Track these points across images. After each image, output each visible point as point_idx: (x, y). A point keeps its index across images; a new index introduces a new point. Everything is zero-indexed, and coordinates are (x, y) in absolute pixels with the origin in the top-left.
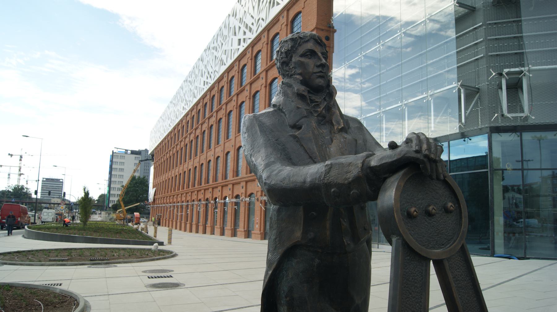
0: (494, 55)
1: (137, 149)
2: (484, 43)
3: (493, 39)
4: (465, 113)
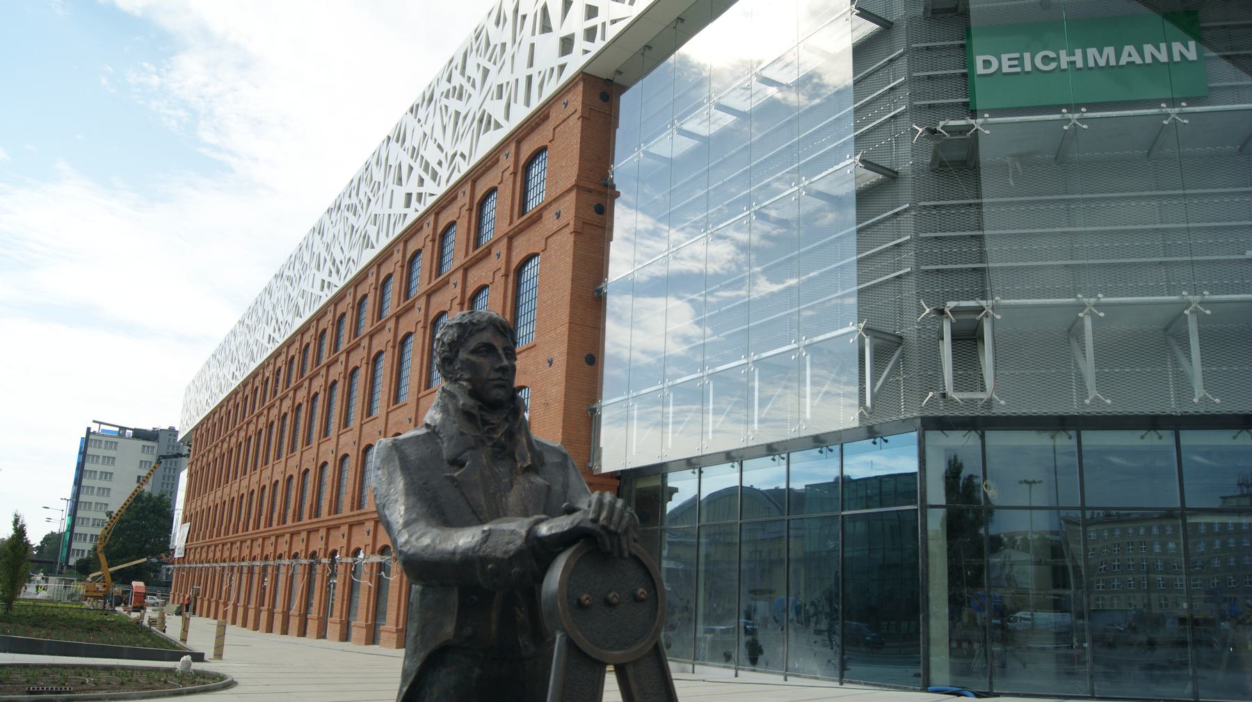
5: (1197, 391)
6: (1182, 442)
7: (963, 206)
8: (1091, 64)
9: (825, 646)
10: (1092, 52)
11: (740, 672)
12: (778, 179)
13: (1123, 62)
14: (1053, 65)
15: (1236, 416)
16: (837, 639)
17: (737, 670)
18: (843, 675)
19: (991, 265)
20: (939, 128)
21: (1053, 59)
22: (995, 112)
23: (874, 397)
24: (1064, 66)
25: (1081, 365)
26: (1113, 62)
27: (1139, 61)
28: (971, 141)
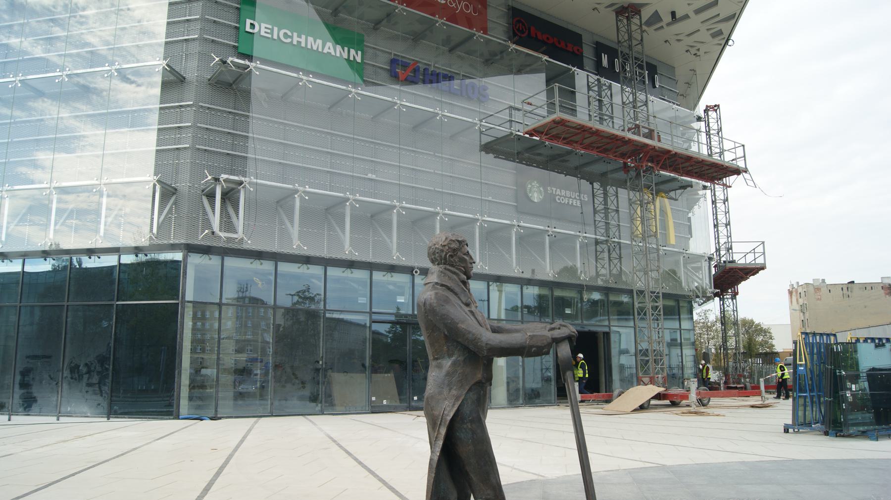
0: (202, 150)
1: (761, 272)
2: (191, 130)
3: (204, 128)
4: (159, 218)
5: (294, 242)
6: (328, 273)
7: (225, 112)
8: (309, 47)
9: (96, 394)
10: (310, 39)
11: (12, 417)
12: (6, 21)
13: (326, 51)
14: (289, 40)
15: (302, 256)
16: (106, 389)
17: (10, 415)
18: (112, 412)
19: (249, 155)
20: (229, 61)
21: (289, 37)
22: (264, 61)
23: (159, 228)
24: (295, 43)
25: (234, 219)
26: (320, 50)
27: (333, 54)
28: (243, 74)
